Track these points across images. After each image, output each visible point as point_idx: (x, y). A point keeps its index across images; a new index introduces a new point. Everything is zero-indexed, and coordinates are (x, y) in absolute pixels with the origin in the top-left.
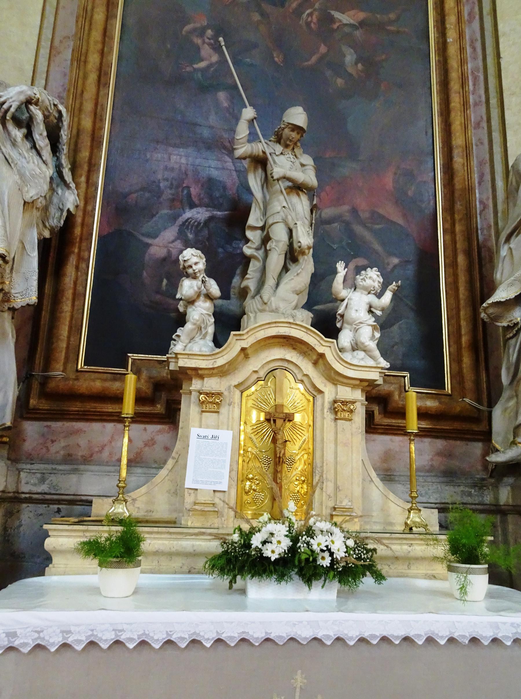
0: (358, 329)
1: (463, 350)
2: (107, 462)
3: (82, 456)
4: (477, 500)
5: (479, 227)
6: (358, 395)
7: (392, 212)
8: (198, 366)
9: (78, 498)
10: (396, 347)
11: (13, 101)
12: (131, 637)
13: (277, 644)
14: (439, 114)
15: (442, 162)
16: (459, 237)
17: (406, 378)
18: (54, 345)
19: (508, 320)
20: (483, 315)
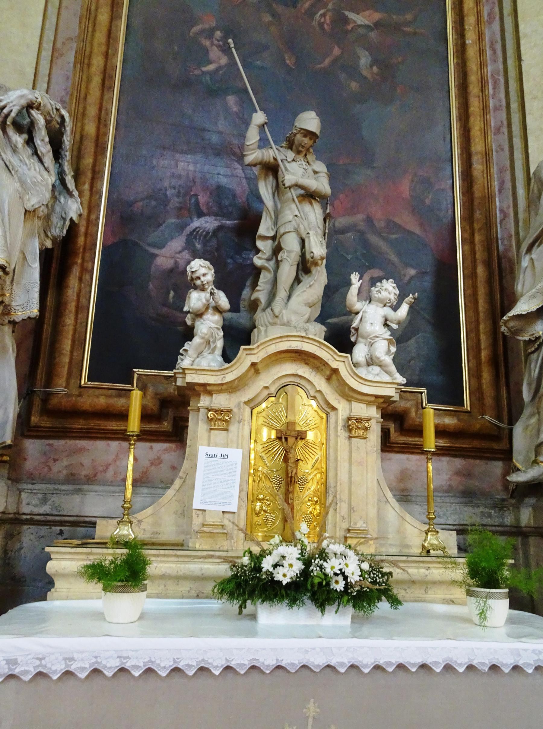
0: (373, 343)
1: (483, 365)
2: (112, 482)
3: (86, 476)
4: (497, 521)
5: (499, 236)
6: (373, 412)
7: (408, 221)
8: (206, 382)
9: (82, 519)
10: (413, 362)
11: (14, 106)
12: (136, 665)
13: (288, 672)
14: (458, 119)
15: (460, 169)
16: (478, 248)
17: (423, 394)
18: (56, 360)
19: (529, 334)
20: (503, 329)
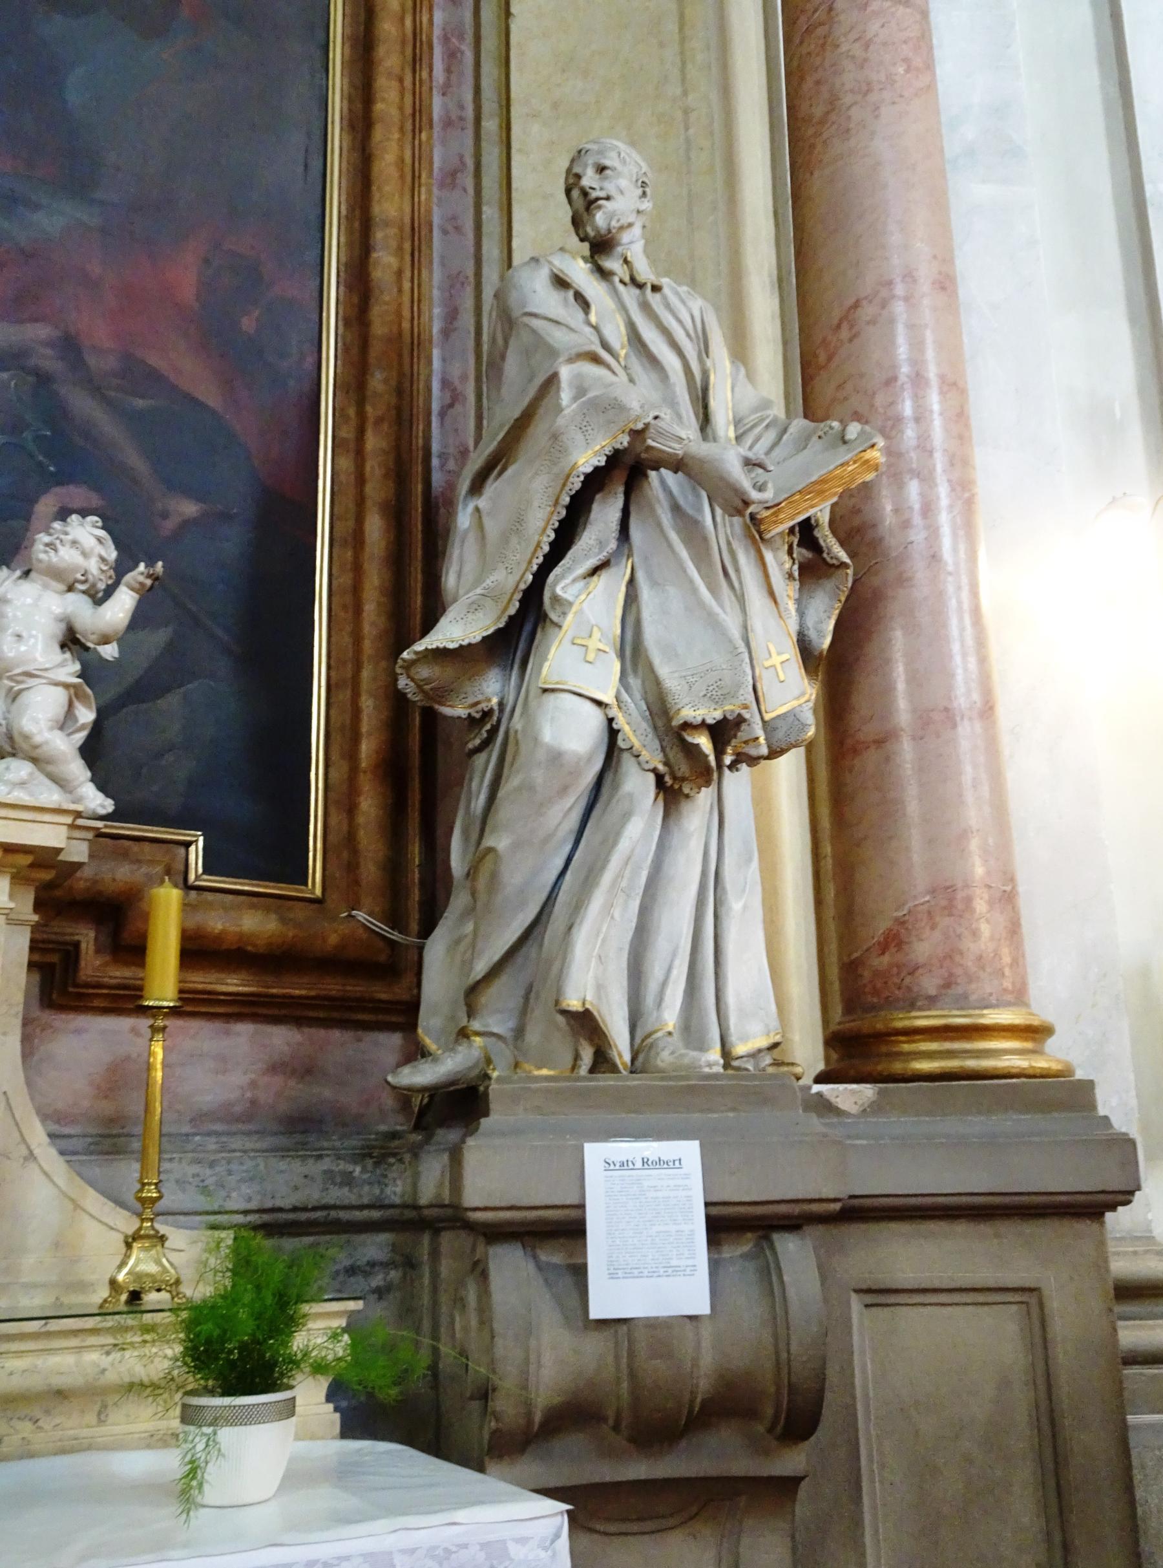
0: (20, 691)
1: (362, 776)
4: (367, 1194)
5: (435, 447)
7: (191, 372)
10: (170, 758)
14: (345, 123)
15: (342, 255)
16: (374, 468)
17: (192, 848)
19: (471, 700)
20: (402, 682)
